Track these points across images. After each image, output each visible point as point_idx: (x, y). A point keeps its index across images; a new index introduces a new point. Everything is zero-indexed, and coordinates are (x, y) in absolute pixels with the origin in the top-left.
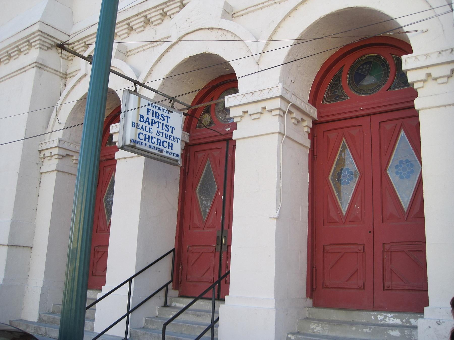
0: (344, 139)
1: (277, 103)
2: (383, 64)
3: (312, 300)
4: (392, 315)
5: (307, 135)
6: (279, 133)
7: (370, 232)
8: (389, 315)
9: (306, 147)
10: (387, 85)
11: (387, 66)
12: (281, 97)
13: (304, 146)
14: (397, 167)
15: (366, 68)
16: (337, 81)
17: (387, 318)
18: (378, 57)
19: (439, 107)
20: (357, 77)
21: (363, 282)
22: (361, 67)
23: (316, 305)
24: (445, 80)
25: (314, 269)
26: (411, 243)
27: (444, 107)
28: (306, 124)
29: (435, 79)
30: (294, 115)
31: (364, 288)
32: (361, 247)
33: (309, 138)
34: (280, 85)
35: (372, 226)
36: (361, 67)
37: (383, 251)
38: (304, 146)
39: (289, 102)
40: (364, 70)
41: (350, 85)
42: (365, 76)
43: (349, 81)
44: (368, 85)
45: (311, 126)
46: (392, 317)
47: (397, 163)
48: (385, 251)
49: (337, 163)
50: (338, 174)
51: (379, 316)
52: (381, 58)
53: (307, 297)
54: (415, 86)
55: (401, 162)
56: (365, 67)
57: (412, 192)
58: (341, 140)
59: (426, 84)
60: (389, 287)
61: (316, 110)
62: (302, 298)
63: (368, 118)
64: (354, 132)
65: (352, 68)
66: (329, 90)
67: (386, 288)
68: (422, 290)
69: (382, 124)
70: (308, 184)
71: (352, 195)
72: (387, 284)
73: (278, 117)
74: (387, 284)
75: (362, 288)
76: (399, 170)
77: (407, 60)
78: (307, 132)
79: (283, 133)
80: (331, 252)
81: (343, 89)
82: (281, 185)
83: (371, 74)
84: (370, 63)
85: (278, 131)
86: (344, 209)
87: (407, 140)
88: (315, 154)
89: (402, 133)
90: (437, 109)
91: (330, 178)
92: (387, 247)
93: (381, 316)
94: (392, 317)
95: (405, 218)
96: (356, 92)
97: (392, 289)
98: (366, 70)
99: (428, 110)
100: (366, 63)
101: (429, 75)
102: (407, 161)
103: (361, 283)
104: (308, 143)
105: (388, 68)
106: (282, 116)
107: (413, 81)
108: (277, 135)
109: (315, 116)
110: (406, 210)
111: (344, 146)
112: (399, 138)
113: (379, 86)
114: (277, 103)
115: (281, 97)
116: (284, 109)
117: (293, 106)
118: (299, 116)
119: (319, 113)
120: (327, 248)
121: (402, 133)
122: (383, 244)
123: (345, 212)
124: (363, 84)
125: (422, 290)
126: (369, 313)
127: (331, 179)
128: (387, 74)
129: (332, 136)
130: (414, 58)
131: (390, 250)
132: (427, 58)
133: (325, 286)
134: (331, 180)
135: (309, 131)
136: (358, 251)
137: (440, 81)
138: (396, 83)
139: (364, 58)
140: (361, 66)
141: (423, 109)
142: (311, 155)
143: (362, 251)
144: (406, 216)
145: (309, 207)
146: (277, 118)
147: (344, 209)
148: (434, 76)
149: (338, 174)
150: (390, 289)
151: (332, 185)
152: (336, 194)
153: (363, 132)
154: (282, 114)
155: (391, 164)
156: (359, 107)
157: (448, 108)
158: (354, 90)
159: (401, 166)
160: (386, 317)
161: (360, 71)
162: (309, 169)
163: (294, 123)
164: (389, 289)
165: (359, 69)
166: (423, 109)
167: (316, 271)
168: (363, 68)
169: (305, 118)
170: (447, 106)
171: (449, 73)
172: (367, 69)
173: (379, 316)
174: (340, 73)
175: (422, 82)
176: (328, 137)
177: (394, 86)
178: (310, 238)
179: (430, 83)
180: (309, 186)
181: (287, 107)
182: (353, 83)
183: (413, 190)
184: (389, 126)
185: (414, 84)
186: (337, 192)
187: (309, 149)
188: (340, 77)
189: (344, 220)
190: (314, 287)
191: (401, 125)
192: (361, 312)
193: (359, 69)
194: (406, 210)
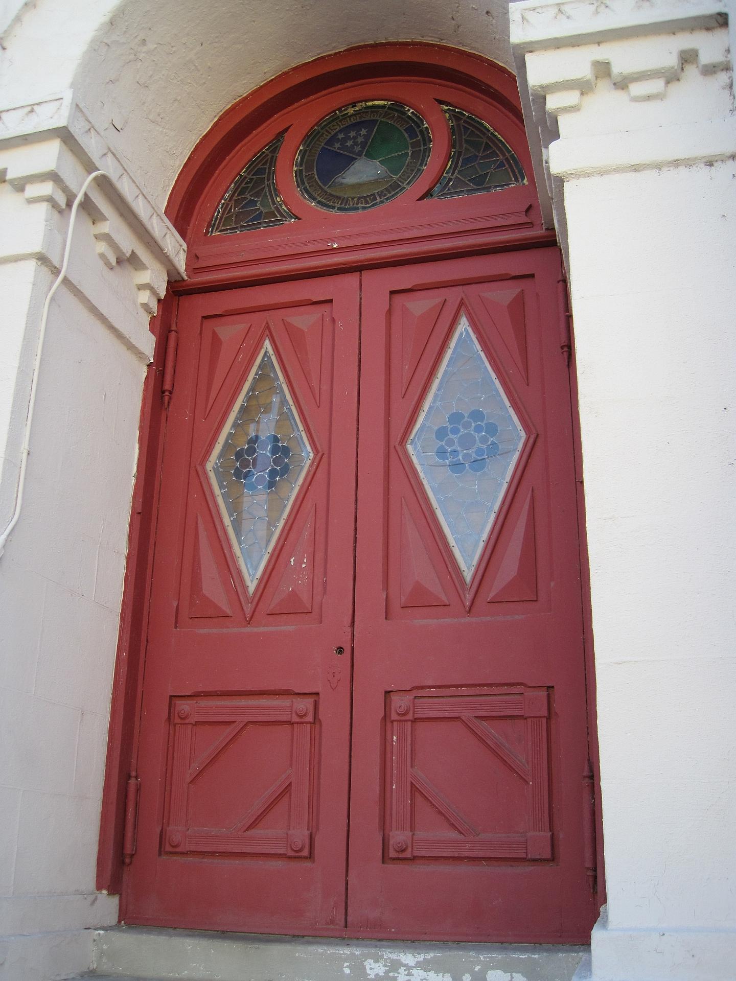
0: (267, 344)
1: (48, 156)
2: (410, 130)
3: (115, 901)
4: (421, 958)
5: (146, 319)
6: (42, 259)
7: (340, 650)
8: (409, 958)
9: (139, 354)
10: (422, 184)
11: (424, 133)
12: (65, 135)
13: (131, 347)
14: (441, 433)
15: (355, 138)
16: (260, 171)
17: (402, 970)
18: (398, 107)
19: (636, 168)
20: (325, 164)
21: (307, 833)
22: (341, 136)
23: (130, 918)
24: (656, 86)
25: (132, 781)
26: (486, 690)
27: (654, 172)
28: (144, 277)
29: (622, 84)
30: (104, 228)
31: (311, 856)
32: (304, 705)
33: (152, 329)
34: (68, 96)
35: (349, 630)
36: (341, 136)
37: (385, 718)
38: (131, 347)
39: (90, 167)
40: (349, 143)
41: (300, 183)
42: (350, 160)
43: (299, 174)
44: (360, 185)
45: (163, 294)
46: (419, 965)
47: (443, 420)
48: (394, 716)
49: (237, 419)
50: (239, 455)
51: (369, 964)
52: (404, 113)
53: (99, 887)
54: (553, 103)
55: (456, 418)
56: (352, 134)
57: (493, 516)
58: (259, 345)
59: (589, 100)
60: (403, 851)
61: (185, 246)
62: (78, 892)
63: (351, 280)
64: (303, 320)
65: (310, 138)
66: (233, 195)
67: (393, 854)
68: (523, 860)
69: (398, 299)
70: (133, 480)
71: (282, 522)
72: (398, 837)
73: (44, 207)
74: (398, 837)
75: (305, 853)
76: (450, 443)
77: (528, 15)
78: (145, 306)
79: (56, 262)
80: (197, 723)
81: (277, 196)
82: (25, 446)
83: (370, 156)
84: (371, 124)
85: (37, 248)
86: (252, 576)
87: (479, 347)
88: (167, 386)
89: (463, 325)
90: (631, 175)
91: (210, 466)
92: (400, 702)
93: (376, 961)
94: (419, 965)
95: (468, 604)
96: (319, 202)
97: (414, 859)
98: (356, 144)
99: (596, 179)
100: (359, 123)
101: (603, 69)
102: (477, 415)
103: (300, 835)
104: (147, 343)
105: (426, 140)
106: (61, 212)
107: (545, 82)
108: (32, 264)
109: (181, 263)
110: (468, 575)
111: (264, 376)
112: (453, 344)
113: (395, 187)
114: (48, 156)
115: (65, 135)
116: (72, 185)
117: (104, 184)
118: (128, 243)
119: (192, 257)
120: (184, 706)
121: (463, 325)
122: (387, 693)
123: (255, 582)
124: (344, 181)
125: (523, 860)
126: (331, 950)
127: (216, 470)
128: (421, 155)
129: (229, 332)
130: (553, 11)
131: (410, 717)
132: (597, 12)
133: (168, 848)
134: (212, 476)
135: (154, 306)
136: (295, 719)
137: (637, 89)
138: (450, 180)
139: (351, 111)
140: (340, 131)
141: (577, 175)
142: (151, 386)
143: (310, 718)
144: (468, 597)
145: (129, 558)
146: (43, 209)
147: (252, 576)
148: (616, 69)
149: (239, 455)
150: (409, 856)
151: (217, 491)
152: (227, 521)
153: (333, 320)
154: (62, 200)
155: (423, 425)
156: (328, 240)
157: (669, 174)
158: (314, 199)
159: (455, 431)
160: (395, 966)
161: (337, 145)
162: (141, 428)
163: (102, 256)
164: (404, 858)
165: (330, 142)
166: (577, 175)
167: (138, 790)
168: (344, 140)
169: (144, 255)
170: (665, 169)
171: (672, 61)
172: (360, 140)
173: (369, 964)
174: (273, 151)
175: (576, 93)
176: (215, 335)
177: (442, 190)
178: (124, 670)
179: (605, 99)
180: (136, 486)
181: (82, 184)
182: (310, 178)
183: (496, 508)
184: (419, 305)
185: (548, 97)
186: (231, 515)
187: (149, 366)
188: (273, 161)
189: (248, 609)
190: (128, 849)
191: (462, 304)
192: (300, 948)
193: (330, 142)
194: (468, 575)
